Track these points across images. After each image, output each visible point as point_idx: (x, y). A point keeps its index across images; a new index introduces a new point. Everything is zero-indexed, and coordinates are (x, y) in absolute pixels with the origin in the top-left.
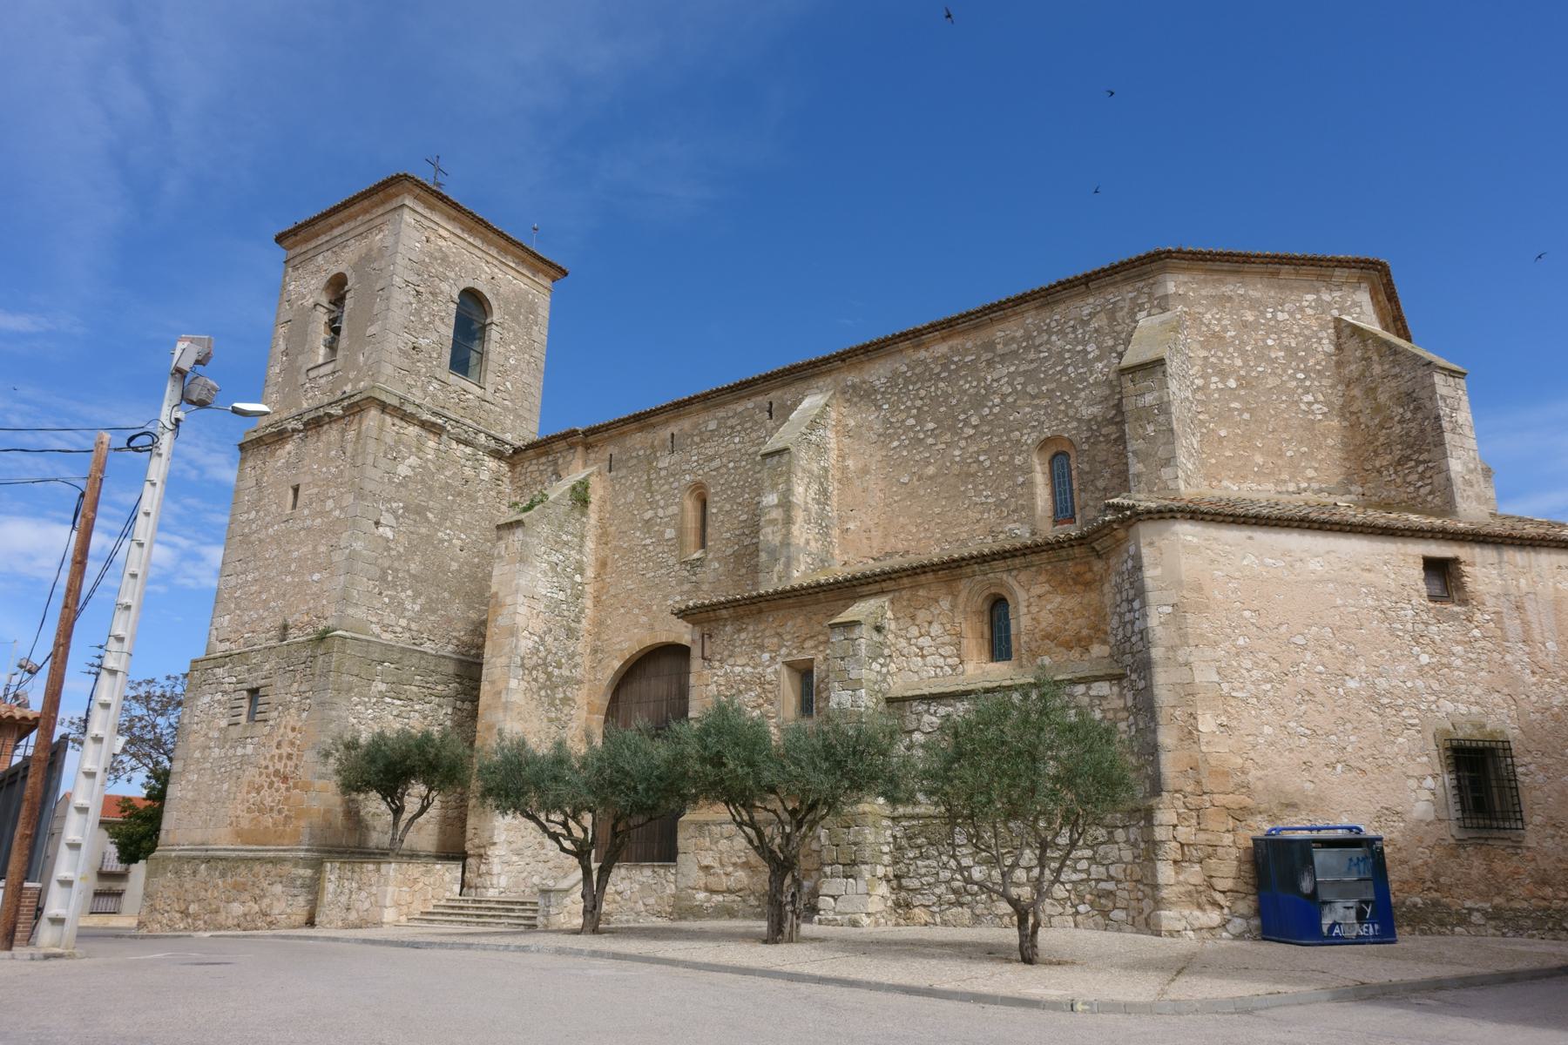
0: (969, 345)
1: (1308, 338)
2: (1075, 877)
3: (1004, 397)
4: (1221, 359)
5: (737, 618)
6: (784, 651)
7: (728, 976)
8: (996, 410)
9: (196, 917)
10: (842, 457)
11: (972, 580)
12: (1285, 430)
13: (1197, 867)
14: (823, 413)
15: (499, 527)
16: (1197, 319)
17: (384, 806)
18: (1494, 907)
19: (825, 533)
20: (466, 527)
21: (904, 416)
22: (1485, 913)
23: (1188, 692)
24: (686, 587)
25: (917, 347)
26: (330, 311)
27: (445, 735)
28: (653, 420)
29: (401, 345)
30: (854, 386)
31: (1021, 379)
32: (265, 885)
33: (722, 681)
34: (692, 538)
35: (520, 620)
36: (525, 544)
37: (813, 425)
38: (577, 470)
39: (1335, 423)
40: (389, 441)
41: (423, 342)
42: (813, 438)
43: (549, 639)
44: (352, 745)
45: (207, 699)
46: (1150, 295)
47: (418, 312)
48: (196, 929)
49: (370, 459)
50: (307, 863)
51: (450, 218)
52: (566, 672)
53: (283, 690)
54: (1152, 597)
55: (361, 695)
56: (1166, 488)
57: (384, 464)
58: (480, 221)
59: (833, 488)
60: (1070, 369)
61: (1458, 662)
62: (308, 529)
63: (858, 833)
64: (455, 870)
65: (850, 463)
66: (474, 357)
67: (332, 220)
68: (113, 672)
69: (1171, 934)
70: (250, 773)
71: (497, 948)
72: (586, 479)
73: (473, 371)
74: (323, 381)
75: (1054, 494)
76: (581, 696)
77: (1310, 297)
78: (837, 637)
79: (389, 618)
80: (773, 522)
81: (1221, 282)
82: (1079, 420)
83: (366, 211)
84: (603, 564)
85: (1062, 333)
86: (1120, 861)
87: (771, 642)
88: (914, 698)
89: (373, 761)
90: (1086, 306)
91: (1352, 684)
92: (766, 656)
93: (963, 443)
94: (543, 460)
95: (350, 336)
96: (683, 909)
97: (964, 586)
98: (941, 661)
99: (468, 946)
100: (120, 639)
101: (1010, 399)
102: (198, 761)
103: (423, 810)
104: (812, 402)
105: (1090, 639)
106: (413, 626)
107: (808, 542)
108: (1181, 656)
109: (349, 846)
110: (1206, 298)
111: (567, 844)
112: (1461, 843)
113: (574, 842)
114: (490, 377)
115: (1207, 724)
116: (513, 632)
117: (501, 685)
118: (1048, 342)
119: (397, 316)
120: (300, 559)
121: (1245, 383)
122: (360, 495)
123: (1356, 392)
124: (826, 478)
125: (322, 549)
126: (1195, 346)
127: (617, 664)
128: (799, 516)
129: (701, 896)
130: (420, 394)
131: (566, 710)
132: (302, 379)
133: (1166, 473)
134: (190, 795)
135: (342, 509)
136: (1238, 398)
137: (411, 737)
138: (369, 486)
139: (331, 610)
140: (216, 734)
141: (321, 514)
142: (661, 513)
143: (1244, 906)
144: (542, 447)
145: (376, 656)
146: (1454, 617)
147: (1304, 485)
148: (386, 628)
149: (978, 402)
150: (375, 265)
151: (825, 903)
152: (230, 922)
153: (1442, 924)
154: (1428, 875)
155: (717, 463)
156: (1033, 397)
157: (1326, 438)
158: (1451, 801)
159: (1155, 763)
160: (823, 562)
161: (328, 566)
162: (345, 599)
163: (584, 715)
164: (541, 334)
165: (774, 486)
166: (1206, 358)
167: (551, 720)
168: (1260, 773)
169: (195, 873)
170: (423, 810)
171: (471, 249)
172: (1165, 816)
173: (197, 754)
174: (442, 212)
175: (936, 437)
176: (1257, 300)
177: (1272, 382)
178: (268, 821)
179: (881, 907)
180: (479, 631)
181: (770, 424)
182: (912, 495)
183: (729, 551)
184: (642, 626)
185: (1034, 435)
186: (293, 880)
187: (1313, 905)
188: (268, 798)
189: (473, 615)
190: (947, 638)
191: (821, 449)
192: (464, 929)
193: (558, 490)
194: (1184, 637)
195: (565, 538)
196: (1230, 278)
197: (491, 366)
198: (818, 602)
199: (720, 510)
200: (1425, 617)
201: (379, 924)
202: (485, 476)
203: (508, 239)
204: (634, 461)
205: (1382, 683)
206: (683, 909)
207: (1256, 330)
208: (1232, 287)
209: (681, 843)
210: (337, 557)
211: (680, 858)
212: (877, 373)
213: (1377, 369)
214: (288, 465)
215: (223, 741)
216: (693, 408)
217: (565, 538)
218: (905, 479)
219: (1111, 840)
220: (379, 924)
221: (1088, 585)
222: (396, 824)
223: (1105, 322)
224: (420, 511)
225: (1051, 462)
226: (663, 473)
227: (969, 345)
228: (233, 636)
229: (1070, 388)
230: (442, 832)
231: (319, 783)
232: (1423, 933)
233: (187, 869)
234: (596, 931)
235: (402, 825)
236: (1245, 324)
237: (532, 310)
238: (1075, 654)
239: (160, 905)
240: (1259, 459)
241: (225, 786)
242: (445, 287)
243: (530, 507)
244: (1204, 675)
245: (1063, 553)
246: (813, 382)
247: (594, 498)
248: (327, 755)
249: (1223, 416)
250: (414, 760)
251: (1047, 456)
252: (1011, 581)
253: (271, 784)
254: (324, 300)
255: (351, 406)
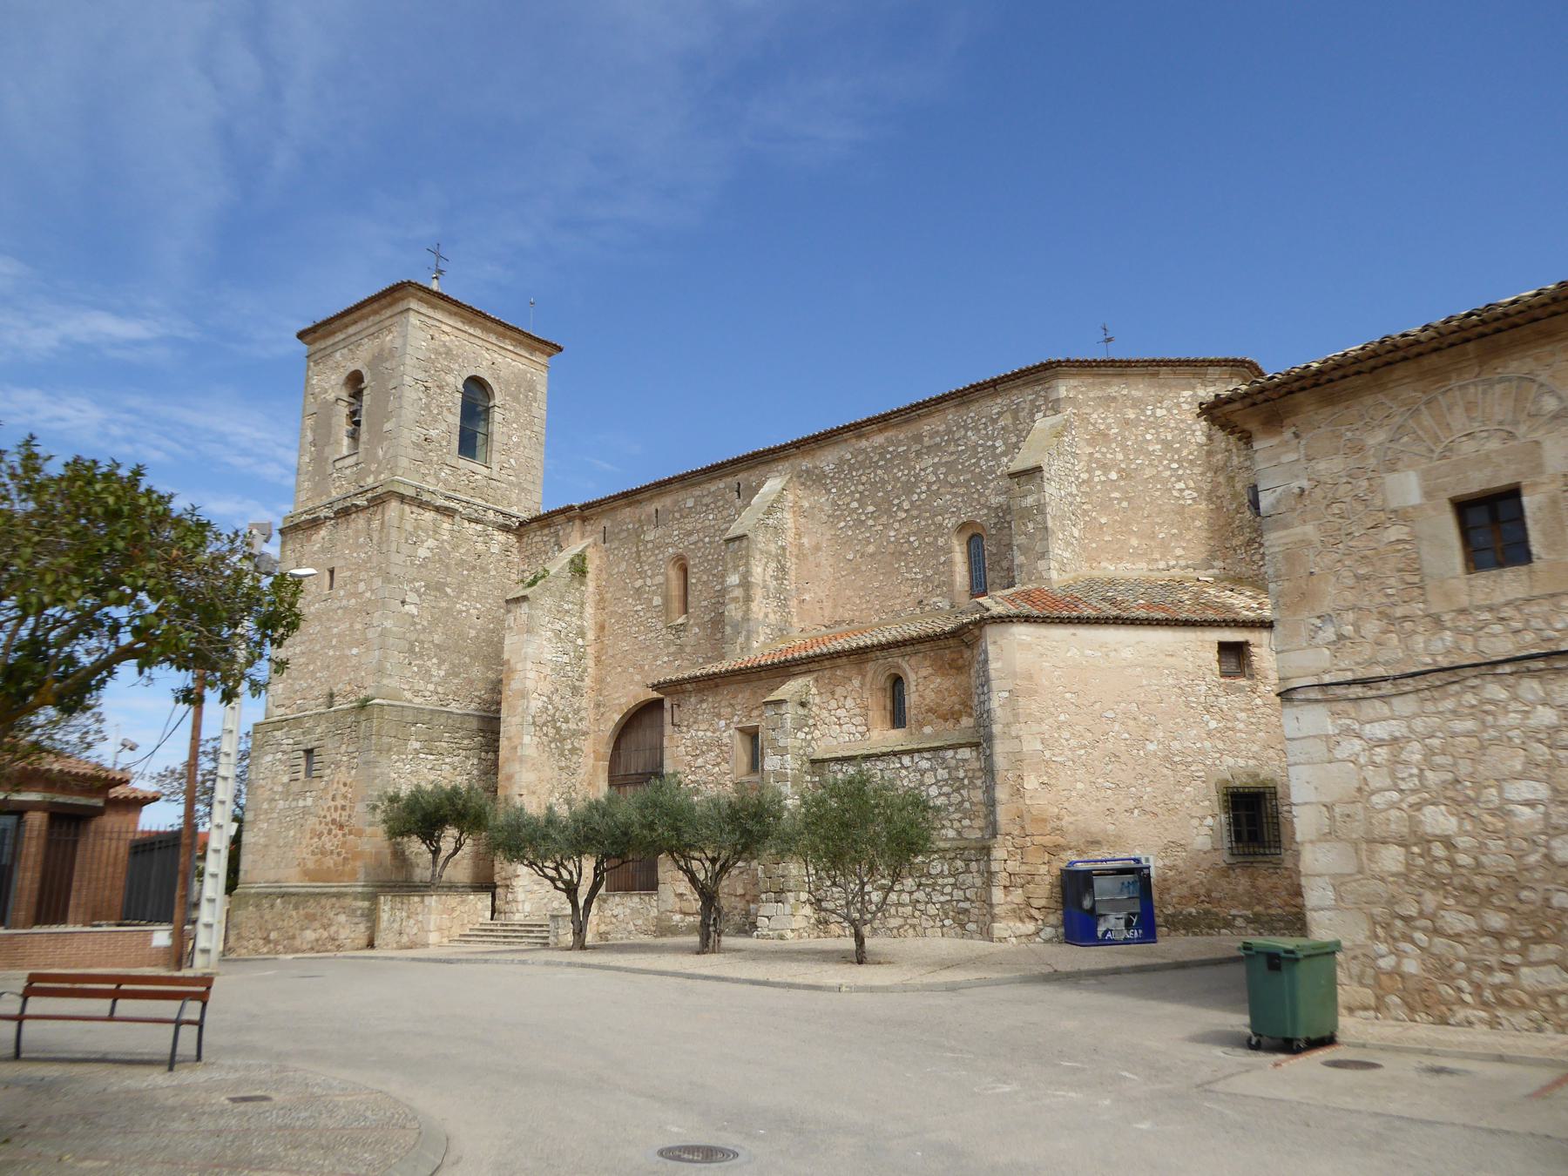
0: (902, 436)
1: (1183, 431)
2: (942, 899)
3: (929, 484)
4: (1104, 454)
5: (700, 691)
6: (736, 719)
7: (745, 986)
8: (923, 496)
9: (276, 943)
10: (799, 535)
11: (879, 665)
12: (1158, 515)
13: (1020, 891)
14: (780, 497)
15: (507, 601)
16: (1085, 419)
17: (424, 847)
18: (1255, 914)
19: (783, 604)
20: (481, 597)
21: (848, 499)
22: (1246, 918)
23: (1018, 759)
24: (673, 649)
25: (859, 437)
26: (351, 404)
27: (471, 788)
28: (639, 497)
29: (414, 439)
30: (807, 471)
31: (943, 470)
32: (331, 915)
33: (689, 743)
34: (676, 605)
35: (530, 684)
36: (530, 617)
37: (770, 510)
38: (578, 542)
39: (1203, 506)
40: (409, 527)
41: (433, 433)
42: (770, 522)
43: (556, 698)
44: (394, 799)
45: (269, 758)
46: (1046, 398)
47: (427, 406)
48: (277, 953)
49: (394, 547)
50: (364, 896)
51: (450, 313)
52: (572, 726)
53: (335, 751)
54: (995, 684)
55: (399, 753)
56: (1041, 577)
57: (405, 549)
58: (479, 313)
59: (791, 563)
60: (982, 462)
61: (1241, 726)
62: (345, 608)
63: (785, 868)
64: (486, 899)
65: (805, 540)
66: (480, 438)
67: (346, 320)
68: (225, 778)
69: (1000, 940)
70: (312, 821)
71: (506, 962)
72: (583, 551)
73: (480, 451)
74: (348, 471)
75: (970, 571)
76: (587, 745)
77: (1187, 393)
78: (769, 713)
79: (422, 685)
80: (735, 600)
81: (1108, 384)
82: (989, 508)
83: (376, 312)
84: (602, 628)
85: (976, 429)
86: (973, 886)
87: (726, 711)
88: (831, 760)
89: (412, 812)
90: (995, 405)
91: (1151, 747)
92: (722, 723)
93: (896, 525)
94: (546, 531)
95: (369, 432)
96: (664, 929)
97: (870, 667)
98: (853, 729)
99: (486, 961)
100: (228, 755)
101: (934, 487)
102: (266, 812)
103: (456, 851)
104: (773, 485)
105: (960, 713)
106: (440, 690)
107: (766, 615)
108: (1014, 731)
109: (400, 882)
110: (1093, 399)
111: (560, 884)
112: (1231, 867)
113: (564, 882)
114: (496, 457)
115: (1031, 783)
116: (523, 694)
117: (516, 741)
118: (965, 436)
119: (409, 413)
120: (339, 635)
121: (1125, 475)
122: (387, 579)
123: (1221, 479)
124: (784, 556)
125: (358, 626)
126: (1082, 444)
127: (617, 717)
128: (758, 594)
129: (677, 917)
130: (433, 481)
131: (575, 758)
132: (330, 469)
133: (1041, 564)
134: (262, 841)
135: (372, 591)
136: (1117, 489)
137: (442, 789)
138: (394, 570)
139: (369, 681)
140: (280, 789)
141: (356, 595)
142: (649, 582)
143: (1054, 919)
144: (544, 521)
145: (410, 719)
146: (1240, 689)
147: (1172, 563)
148: (416, 693)
149: (909, 488)
150: (387, 365)
151: (762, 922)
152: (305, 947)
153: (1211, 927)
154: (1202, 891)
155: (694, 538)
156: (953, 486)
157: (1194, 520)
158: (1225, 834)
159: (993, 813)
160: (782, 631)
161: (363, 642)
162: (380, 671)
163: (591, 762)
164: (540, 409)
165: (736, 568)
166: (1091, 454)
167: (561, 769)
168: (1072, 819)
169: (272, 906)
170: (456, 851)
171: (472, 339)
172: (999, 853)
173: (265, 806)
174: (443, 309)
175: (875, 519)
176: (1140, 400)
177: (1149, 472)
178: (329, 862)
179: (804, 924)
180: (496, 687)
181: (738, 503)
182: (856, 570)
183: (707, 618)
184: (637, 683)
185: (953, 520)
186: (354, 911)
187: (1092, 917)
188: (329, 843)
189: (491, 675)
190: (858, 711)
191: (778, 531)
192: (493, 947)
193: (559, 563)
194: (1016, 715)
195: (566, 607)
196: (1116, 380)
197: (496, 446)
198: (761, 679)
199: (699, 580)
200: (1216, 690)
201: (426, 945)
202: (495, 549)
203: (505, 325)
204: (624, 534)
205: (1176, 745)
206: (664, 928)
207: (1136, 426)
208: (1117, 388)
209: (661, 875)
210: (371, 634)
211: (661, 887)
212: (827, 460)
213: (1235, 461)
214: (323, 550)
215: (286, 794)
216: (673, 487)
217: (566, 607)
218: (850, 557)
219: (967, 871)
220: (426, 945)
221: (959, 669)
222: (435, 862)
223: (1010, 421)
224: (439, 587)
225: (969, 543)
226: (650, 546)
227: (902, 436)
228: (287, 702)
229: (981, 479)
230: (476, 865)
231: (369, 830)
232: (1195, 934)
233: (265, 903)
234: (583, 947)
235: (441, 861)
236: (1127, 422)
237: (531, 387)
238: (949, 724)
239: (245, 933)
240: (1134, 542)
241: (292, 833)
242: (450, 379)
243: (533, 583)
244: (1031, 745)
245: (941, 643)
246: (773, 465)
247: (591, 567)
248: (375, 808)
249: (1105, 506)
250: (446, 810)
251: (965, 537)
252: (905, 665)
253: (330, 832)
254: (344, 395)
255: (374, 498)
